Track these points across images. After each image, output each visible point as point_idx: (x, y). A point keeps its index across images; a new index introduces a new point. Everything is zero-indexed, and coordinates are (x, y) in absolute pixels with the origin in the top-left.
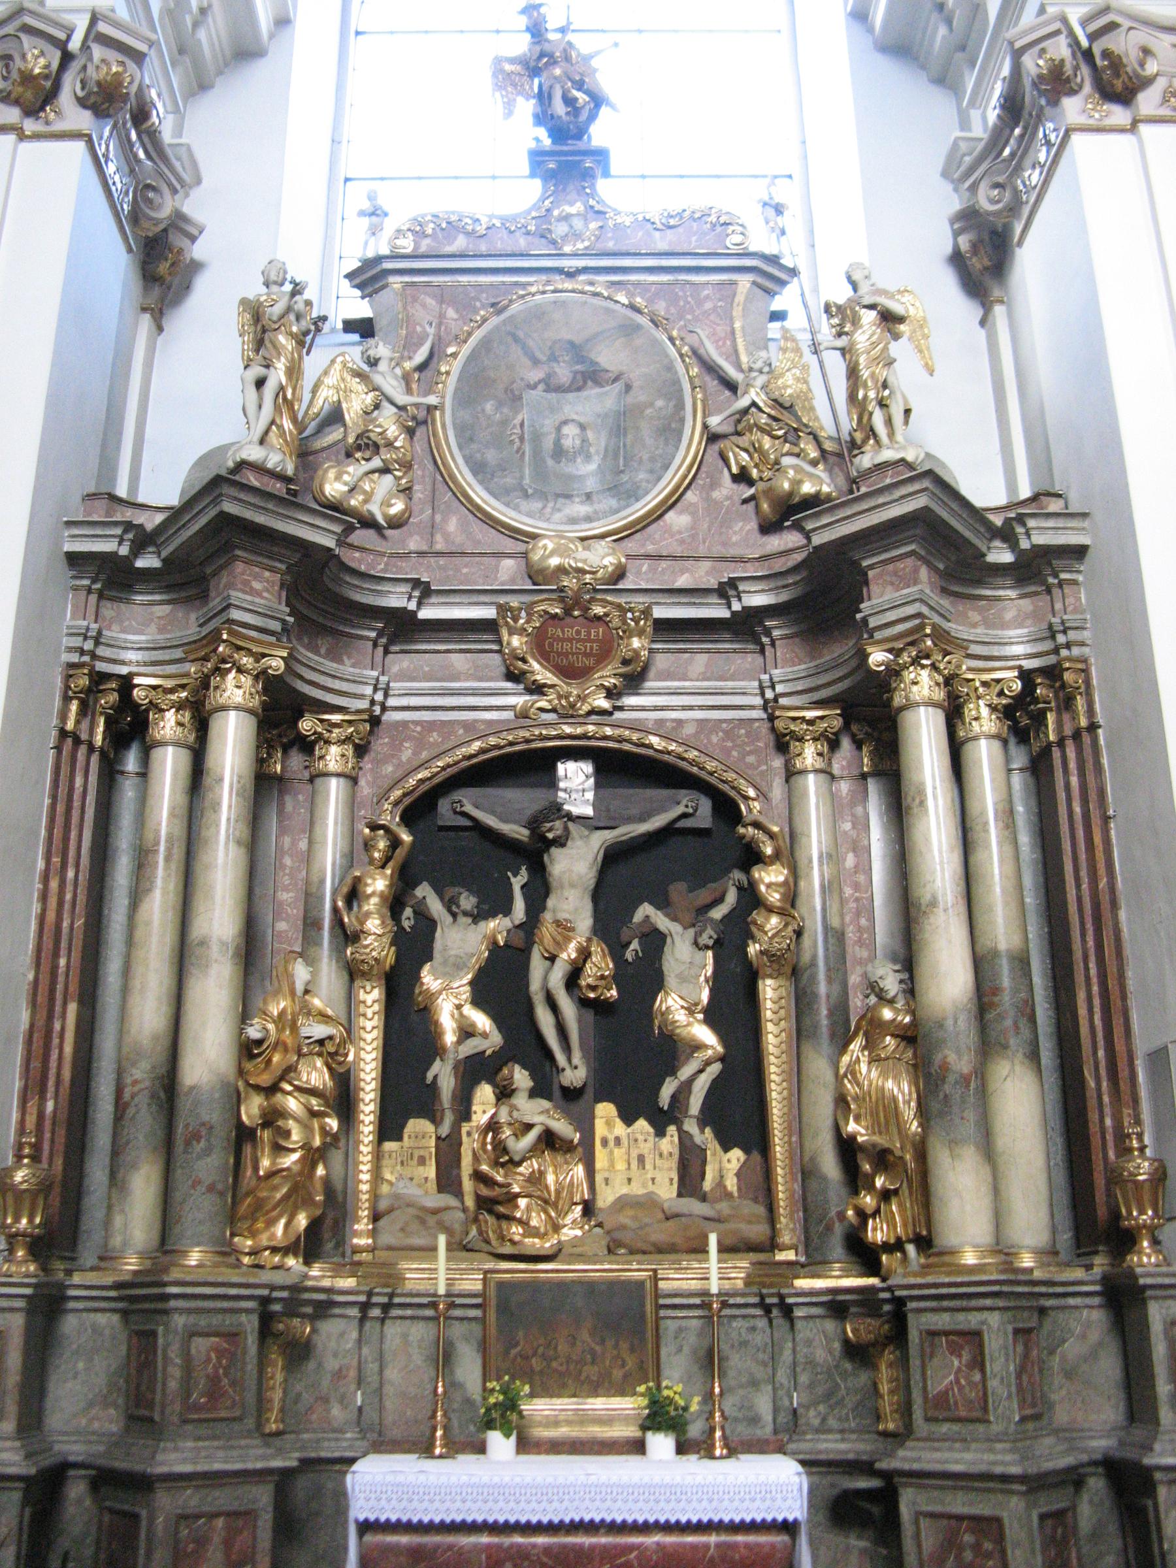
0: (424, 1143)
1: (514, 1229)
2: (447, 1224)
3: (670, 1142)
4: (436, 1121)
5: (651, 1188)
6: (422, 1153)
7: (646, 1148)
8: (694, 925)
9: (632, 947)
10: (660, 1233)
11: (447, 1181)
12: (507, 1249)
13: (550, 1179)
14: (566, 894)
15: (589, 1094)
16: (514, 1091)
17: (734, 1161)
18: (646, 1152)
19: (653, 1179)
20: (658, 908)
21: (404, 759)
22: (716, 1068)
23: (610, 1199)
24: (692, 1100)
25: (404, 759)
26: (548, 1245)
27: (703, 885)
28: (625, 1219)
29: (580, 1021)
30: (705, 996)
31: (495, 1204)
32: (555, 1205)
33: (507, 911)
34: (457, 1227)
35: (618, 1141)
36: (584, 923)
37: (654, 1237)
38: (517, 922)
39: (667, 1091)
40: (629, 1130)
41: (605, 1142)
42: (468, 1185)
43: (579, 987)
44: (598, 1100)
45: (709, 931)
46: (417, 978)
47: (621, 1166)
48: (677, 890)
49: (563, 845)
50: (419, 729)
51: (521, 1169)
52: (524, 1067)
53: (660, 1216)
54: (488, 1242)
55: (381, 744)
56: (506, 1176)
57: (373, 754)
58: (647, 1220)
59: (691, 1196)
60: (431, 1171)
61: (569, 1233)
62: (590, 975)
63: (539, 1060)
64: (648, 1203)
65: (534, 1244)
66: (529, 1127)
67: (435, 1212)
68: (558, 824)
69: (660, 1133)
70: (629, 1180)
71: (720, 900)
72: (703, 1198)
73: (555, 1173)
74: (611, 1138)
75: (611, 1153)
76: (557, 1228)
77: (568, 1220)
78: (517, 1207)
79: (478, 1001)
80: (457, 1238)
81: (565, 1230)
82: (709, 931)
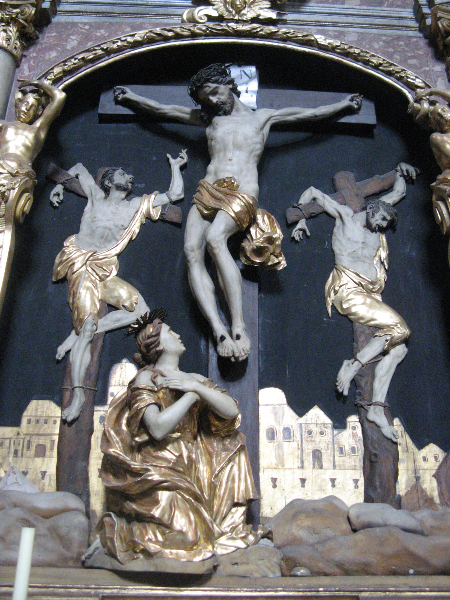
0: (45, 429)
1: (151, 535)
2: (63, 530)
3: (352, 434)
4: (62, 404)
5: (329, 491)
6: (42, 441)
7: (323, 442)
8: (364, 209)
9: (299, 226)
10: (349, 549)
11: (71, 477)
12: (140, 565)
13: (204, 471)
14: (229, 155)
15: (253, 372)
16: (160, 354)
17: (431, 460)
18: (322, 446)
19: (333, 481)
20: (325, 192)
21: (69, 47)
22: (400, 351)
23: (280, 506)
24: (377, 385)
25: (69, 47)
26: (198, 559)
27: (370, 175)
28: (299, 530)
29: (243, 293)
30: (381, 275)
31: (129, 499)
32: (209, 506)
33: (164, 187)
34: (76, 536)
35: (287, 432)
36: (249, 185)
37: (339, 556)
38: (174, 198)
39: (346, 374)
40: (302, 420)
41: (272, 435)
42: (96, 484)
43: (243, 250)
44: (263, 384)
45: (382, 212)
46: (60, 247)
47: (292, 462)
48: (344, 179)
49: (227, 113)
50: (87, 27)
51: (166, 454)
52: (173, 328)
53: (346, 526)
54: (113, 555)
55: (48, 36)
56: (144, 461)
57: (39, 47)
58: (329, 533)
59: (384, 501)
60: (50, 464)
61: (226, 546)
62: (256, 236)
63: (196, 328)
64: (328, 509)
65: (176, 558)
66: (178, 394)
67: (48, 515)
68: (223, 88)
69: (340, 424)
70: (303, 481)
71: (390, 189)
72: (398, 503)
73: (210, 464)
74: (279, 429)
75: (280, 447)
76: (211, 537)
77: (226, 526)
78: (156, 502)
79: (125, 274)
80: (75, 549)
81: (223, 540)
82: (382, 212)
